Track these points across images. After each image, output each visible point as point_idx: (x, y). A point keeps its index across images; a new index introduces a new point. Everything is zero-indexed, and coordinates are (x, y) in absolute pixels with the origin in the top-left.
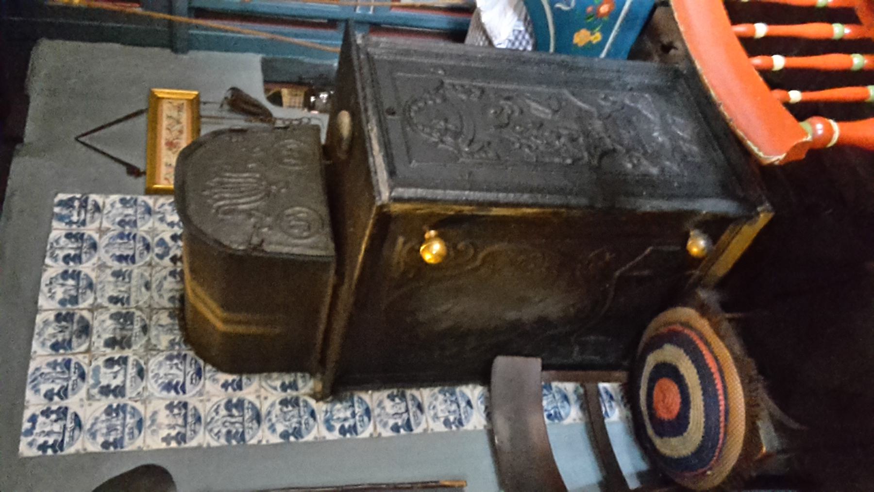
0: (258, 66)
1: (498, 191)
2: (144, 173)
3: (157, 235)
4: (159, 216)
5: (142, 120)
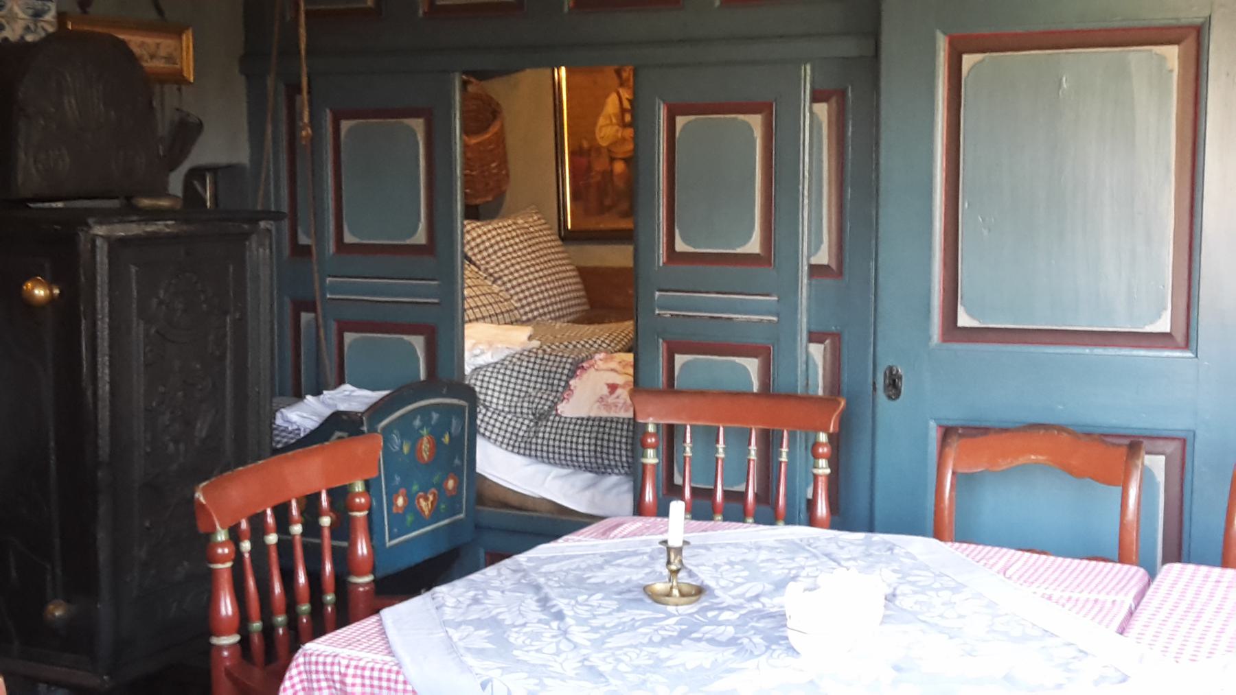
0: (234, 161)
1: (112, 383)
2: (85, 12)
3: (8, 23)
4: (32, 26)
5: (152, 15)
